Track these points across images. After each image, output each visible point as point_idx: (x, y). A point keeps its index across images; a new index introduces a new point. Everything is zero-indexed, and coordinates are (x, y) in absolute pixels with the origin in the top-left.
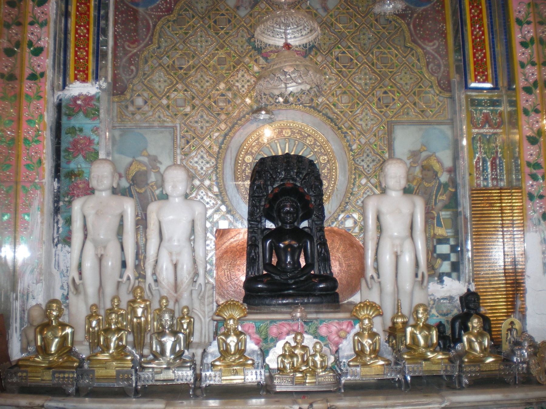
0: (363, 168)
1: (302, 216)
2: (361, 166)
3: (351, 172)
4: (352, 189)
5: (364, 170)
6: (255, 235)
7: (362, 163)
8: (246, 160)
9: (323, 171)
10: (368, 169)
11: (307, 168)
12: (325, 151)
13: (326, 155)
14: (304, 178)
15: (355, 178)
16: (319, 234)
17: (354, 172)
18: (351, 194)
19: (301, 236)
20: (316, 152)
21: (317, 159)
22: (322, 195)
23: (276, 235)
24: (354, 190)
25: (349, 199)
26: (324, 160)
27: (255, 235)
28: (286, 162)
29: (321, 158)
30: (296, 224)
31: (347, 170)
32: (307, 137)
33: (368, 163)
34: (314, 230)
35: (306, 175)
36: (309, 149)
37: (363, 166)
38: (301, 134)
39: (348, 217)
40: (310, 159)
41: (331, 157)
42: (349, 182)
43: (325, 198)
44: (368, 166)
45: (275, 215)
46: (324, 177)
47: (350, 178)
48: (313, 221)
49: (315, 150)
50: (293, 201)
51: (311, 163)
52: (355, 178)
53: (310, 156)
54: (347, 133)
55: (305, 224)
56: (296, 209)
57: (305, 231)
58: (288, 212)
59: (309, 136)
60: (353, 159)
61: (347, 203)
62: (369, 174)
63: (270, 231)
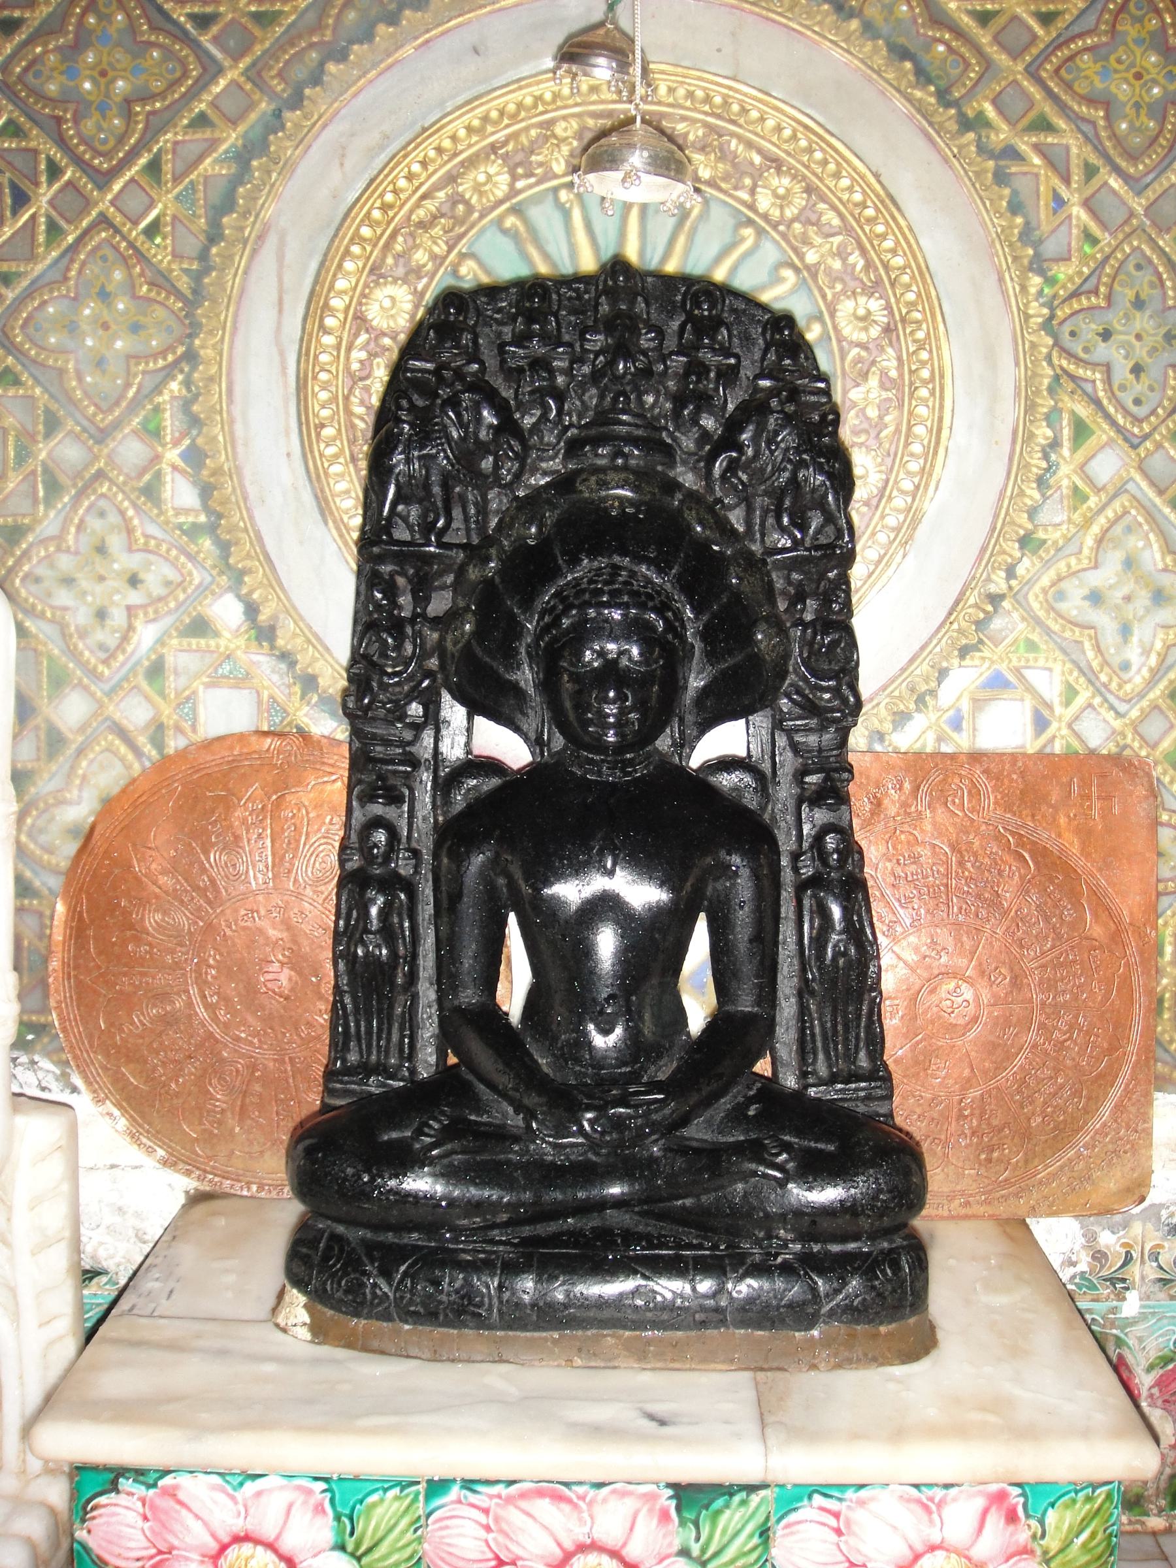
0: (1108, 380)
1: (704, 692)
2: (1094, 365)
3: (1031, 407)
4: (1032, 512)
5: (1113, 396)
6: (390, 812)
7: (1103, 351)
8: (373, 312)
9: (855, 394)
10: (1139, 388)
11: (747, 371)
12: (869, 264)
13: (874, 289)
14: (728, 441)
15: (1055, 444)
16: (814, 818)
17: (1046, 404)
18: (1025, 541)
19: (689, 827)
20: (813, 271)
21: (819, 318)
22: (849, 557)
23: (524, 823)
24: (1043, 517)
25: (1010, 573)
26: (866, 319)
27: (390, 812)
28: (609, 326)
29: (846, 307)
30: (664, 743)
31: (1008, 390)
32: (757, 175)
33: (1141, 352)
34: (785, 792)
35: (733, 426)
36: (768, 247)
37: (1107, 368)
38: (724, 155)
39: (997, 684)
40: (778, 306)
41: (912, 305)
42: (1015, 466)
43: (857, 573)
44: (1137, 370)
45: (526, 676)
46: (856, 433)
47: (1022, 437)
48: (778, 724)
49: (811, 257)
50: (643, 598)
51: (783, 332)
52: (1055, 444)
53: (779, 294)
54: (1017, 156)
55: (728, 739)
56: (667, 654)
57: (713, 792)
58: (611, 672)
59: (776, 164)
60: (1048, 325)
61: (995, 599)
62: (1138, 421)
63: (495, 782)
